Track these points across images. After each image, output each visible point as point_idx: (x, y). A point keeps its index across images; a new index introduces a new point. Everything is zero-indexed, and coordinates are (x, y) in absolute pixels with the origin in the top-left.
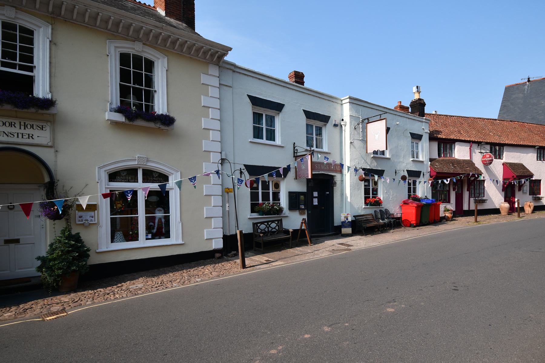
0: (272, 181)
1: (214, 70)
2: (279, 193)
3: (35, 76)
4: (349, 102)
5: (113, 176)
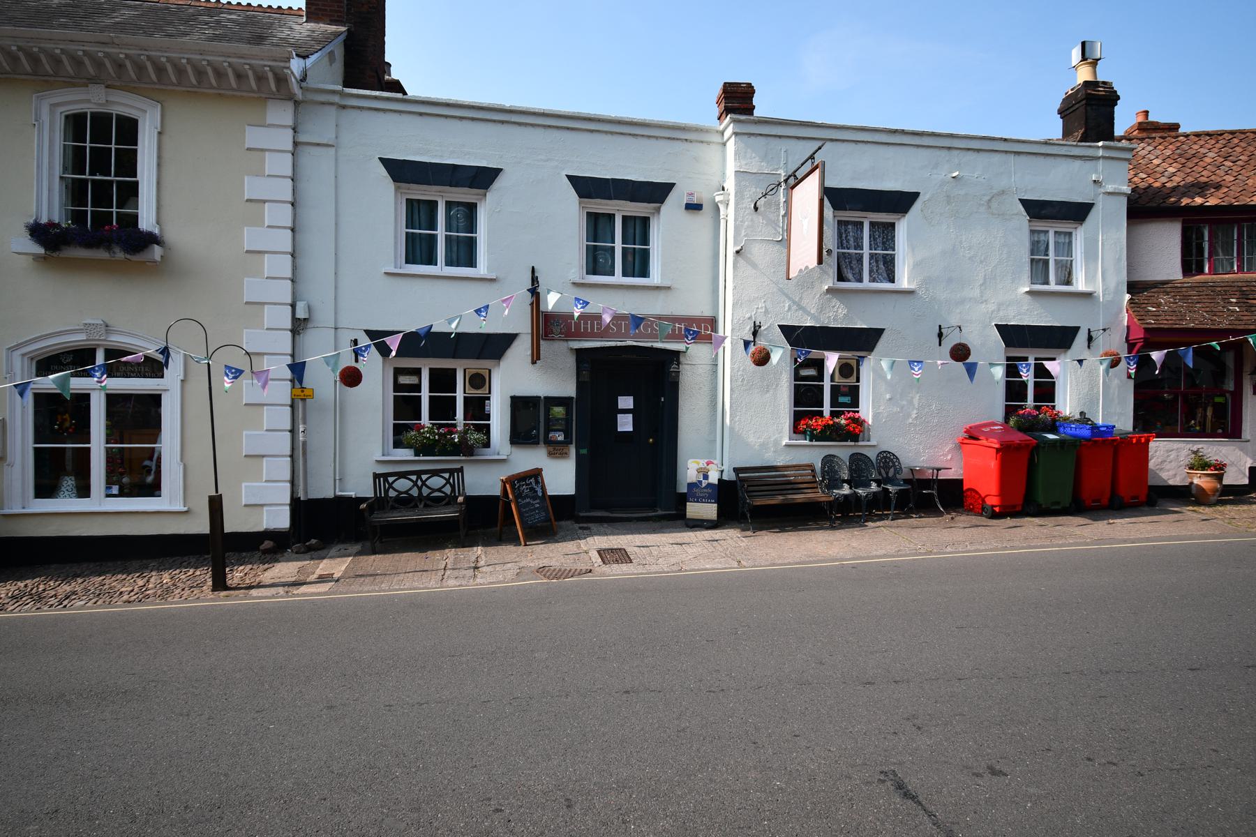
0: (465, 370)
2: (489, 399)
4: (736, 134)
5: (46, 365)
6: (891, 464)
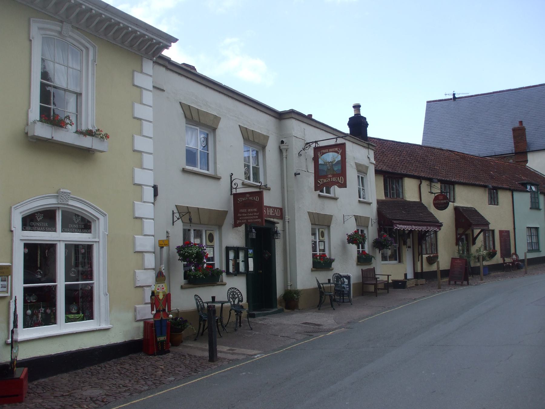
1: (148, 66)
3: (79, 95)
6: (236, 296)
